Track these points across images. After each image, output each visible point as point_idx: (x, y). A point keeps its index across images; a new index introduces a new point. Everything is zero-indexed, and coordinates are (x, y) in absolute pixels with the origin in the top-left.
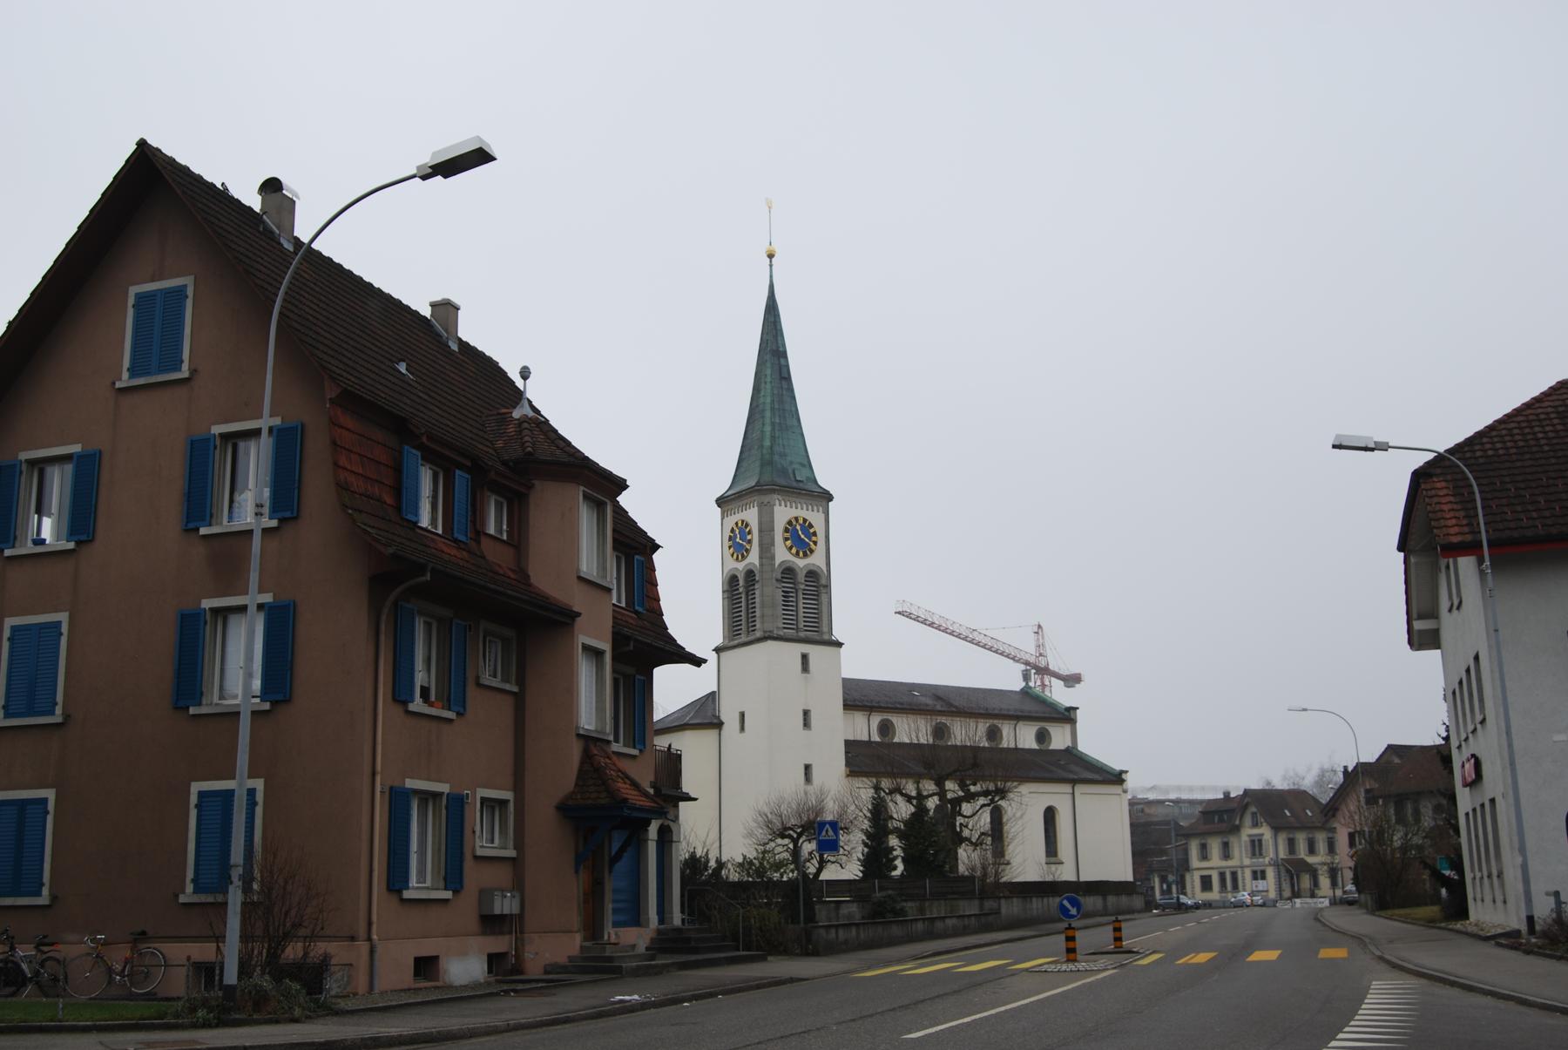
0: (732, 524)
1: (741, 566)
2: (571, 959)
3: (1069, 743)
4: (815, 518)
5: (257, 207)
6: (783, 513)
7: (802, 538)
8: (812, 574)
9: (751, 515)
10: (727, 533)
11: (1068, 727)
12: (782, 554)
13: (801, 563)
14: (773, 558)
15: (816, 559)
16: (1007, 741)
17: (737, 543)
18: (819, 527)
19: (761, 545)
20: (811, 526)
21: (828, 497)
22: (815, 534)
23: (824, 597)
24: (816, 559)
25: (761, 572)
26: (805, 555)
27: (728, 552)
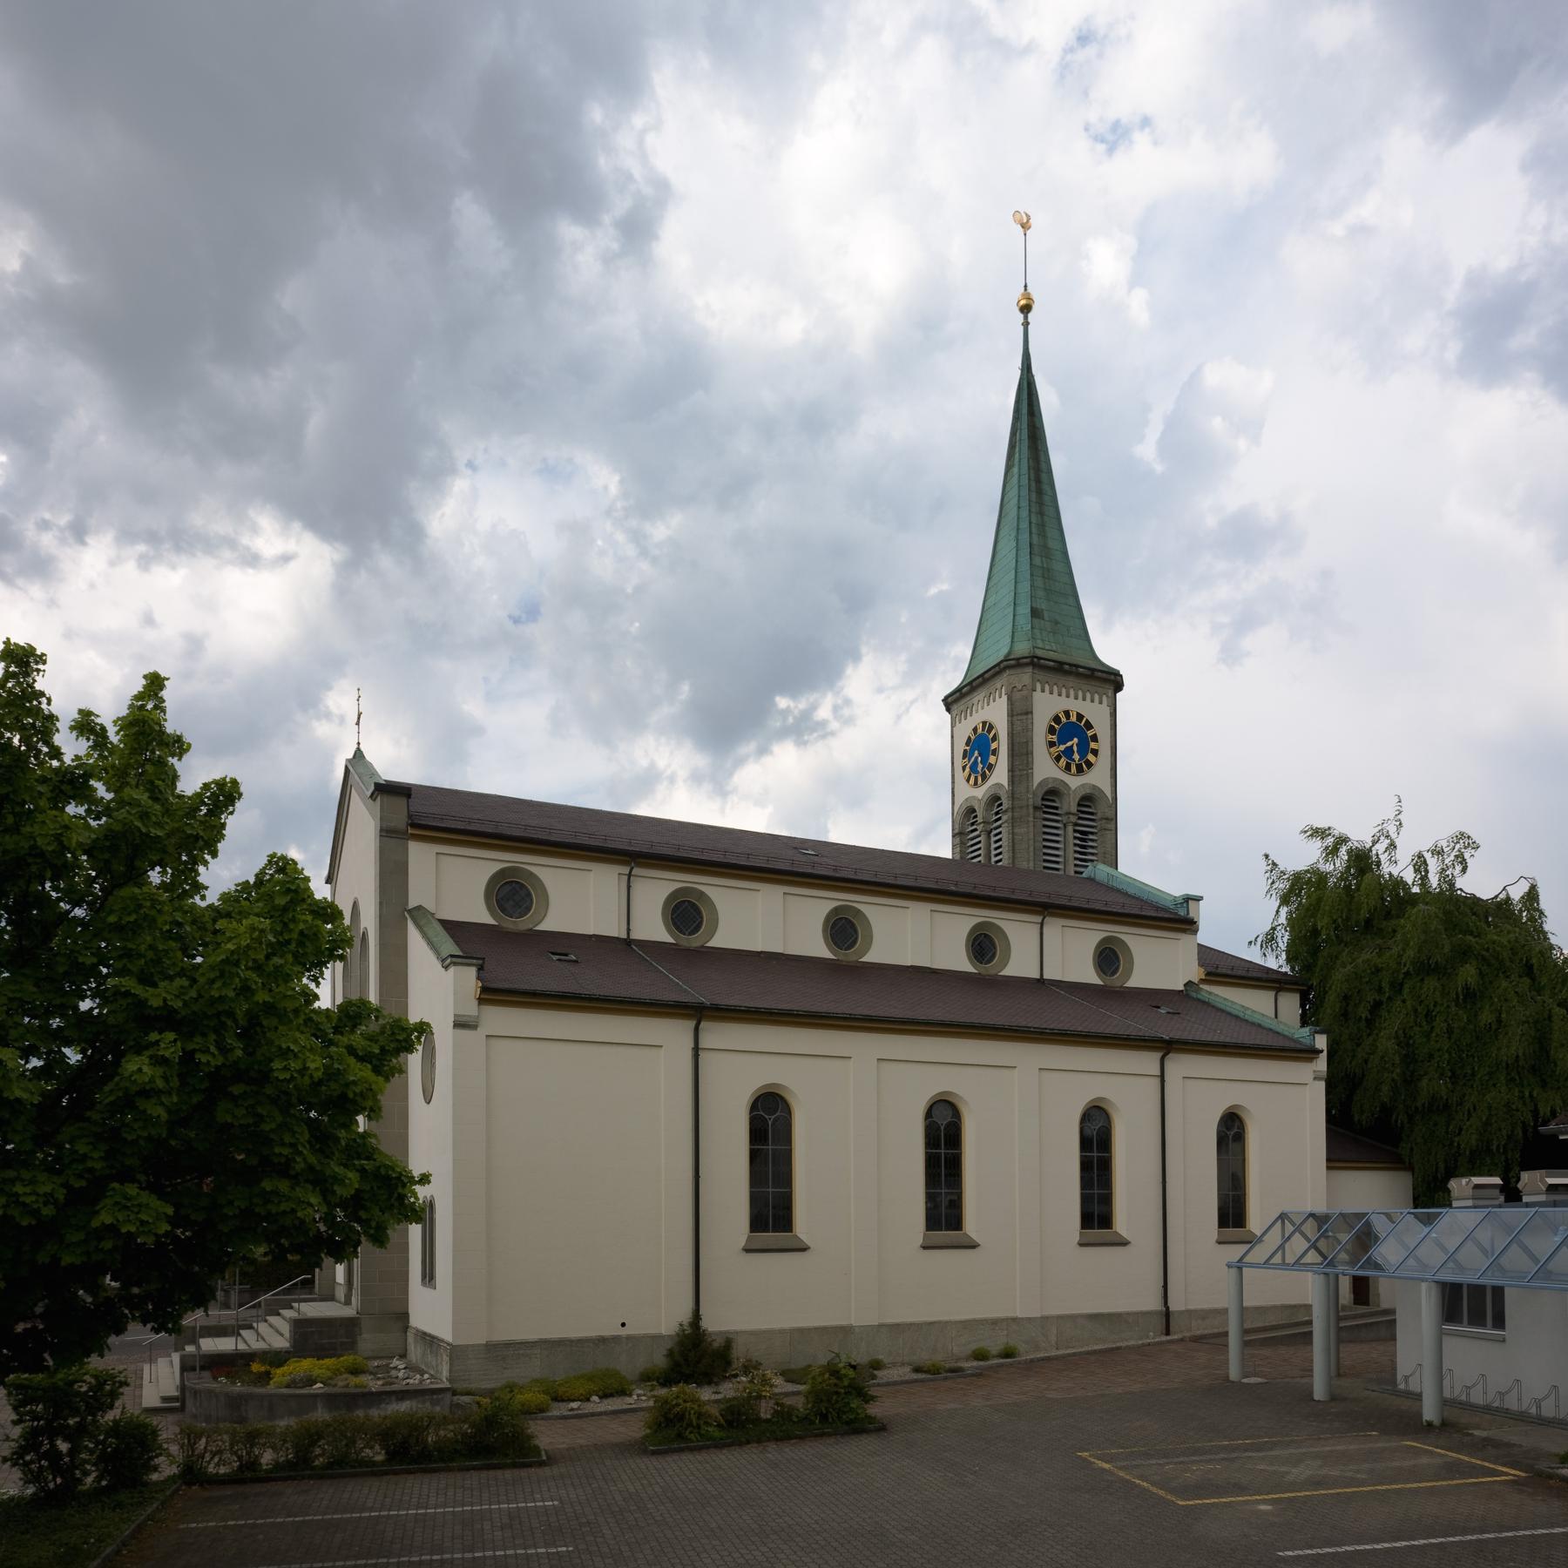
0: (968, 732)
1: (980, 793)
2: (165, 1399)
3: (1497, 1191)
4: (1093, 711)
5: (672, 940)
6: (1048, 704)
7: (1080, 741)
8: (1088, 800)
9: (994, 710)
10: (961, 747)
11: (1447, 1394)
12: (1045, 769)
13: (1074, 782)
14: (1029, 777)
15: (1096, 777)
16: (1020, 963)
17: (976, 752)
18: (1101, 728)
19: (1013, 754)
20: (1089, 726)
21: (1112, 681)
22: (1095, 738)
23: (1042, 458)
24: (1096, 777)
25: (1013, 795)
26: (1080, 770)
27: (961, 776)
